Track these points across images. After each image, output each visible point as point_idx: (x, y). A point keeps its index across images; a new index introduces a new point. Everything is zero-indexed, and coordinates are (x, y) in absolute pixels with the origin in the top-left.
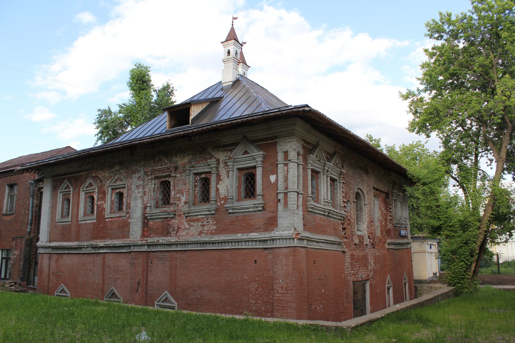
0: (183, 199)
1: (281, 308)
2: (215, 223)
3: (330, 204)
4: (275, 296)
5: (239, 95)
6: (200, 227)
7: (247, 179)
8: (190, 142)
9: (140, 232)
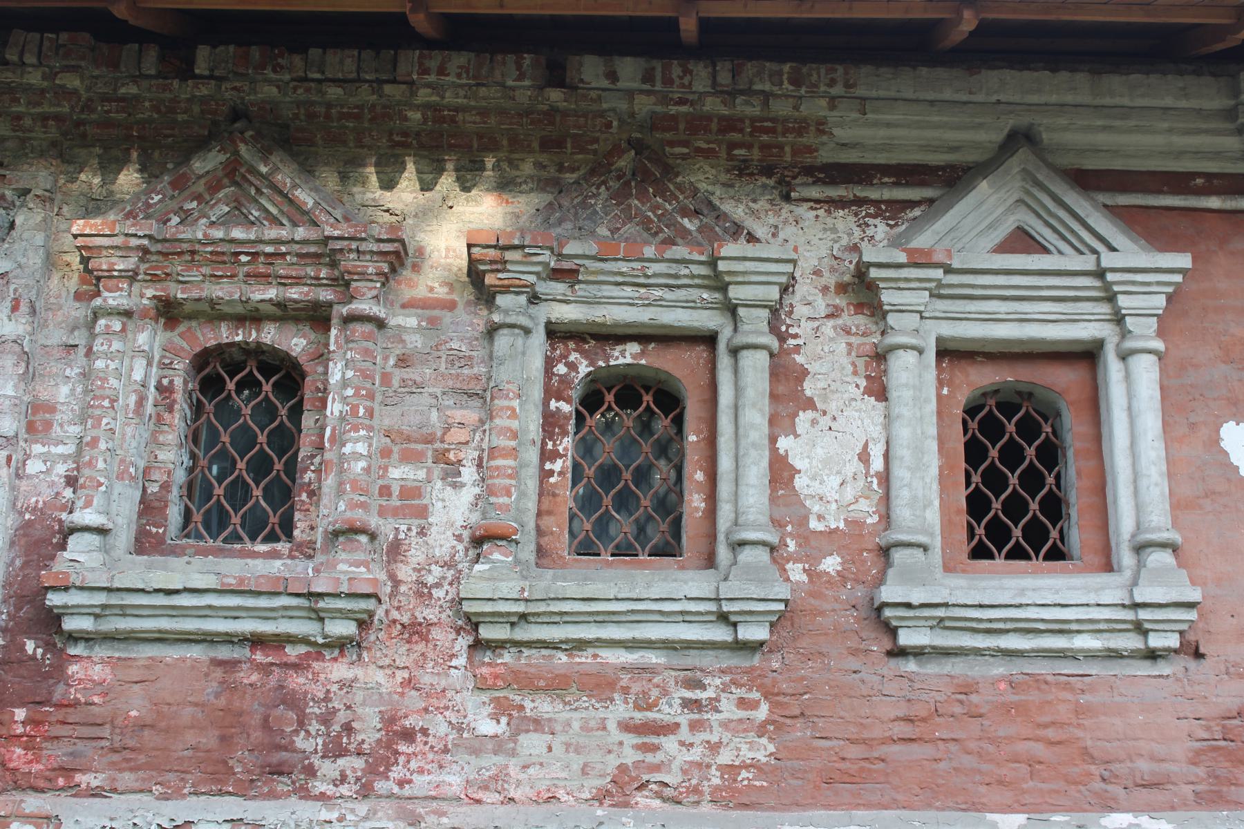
0: (454, 508)
2: (763, 712)
6: (615, 735)
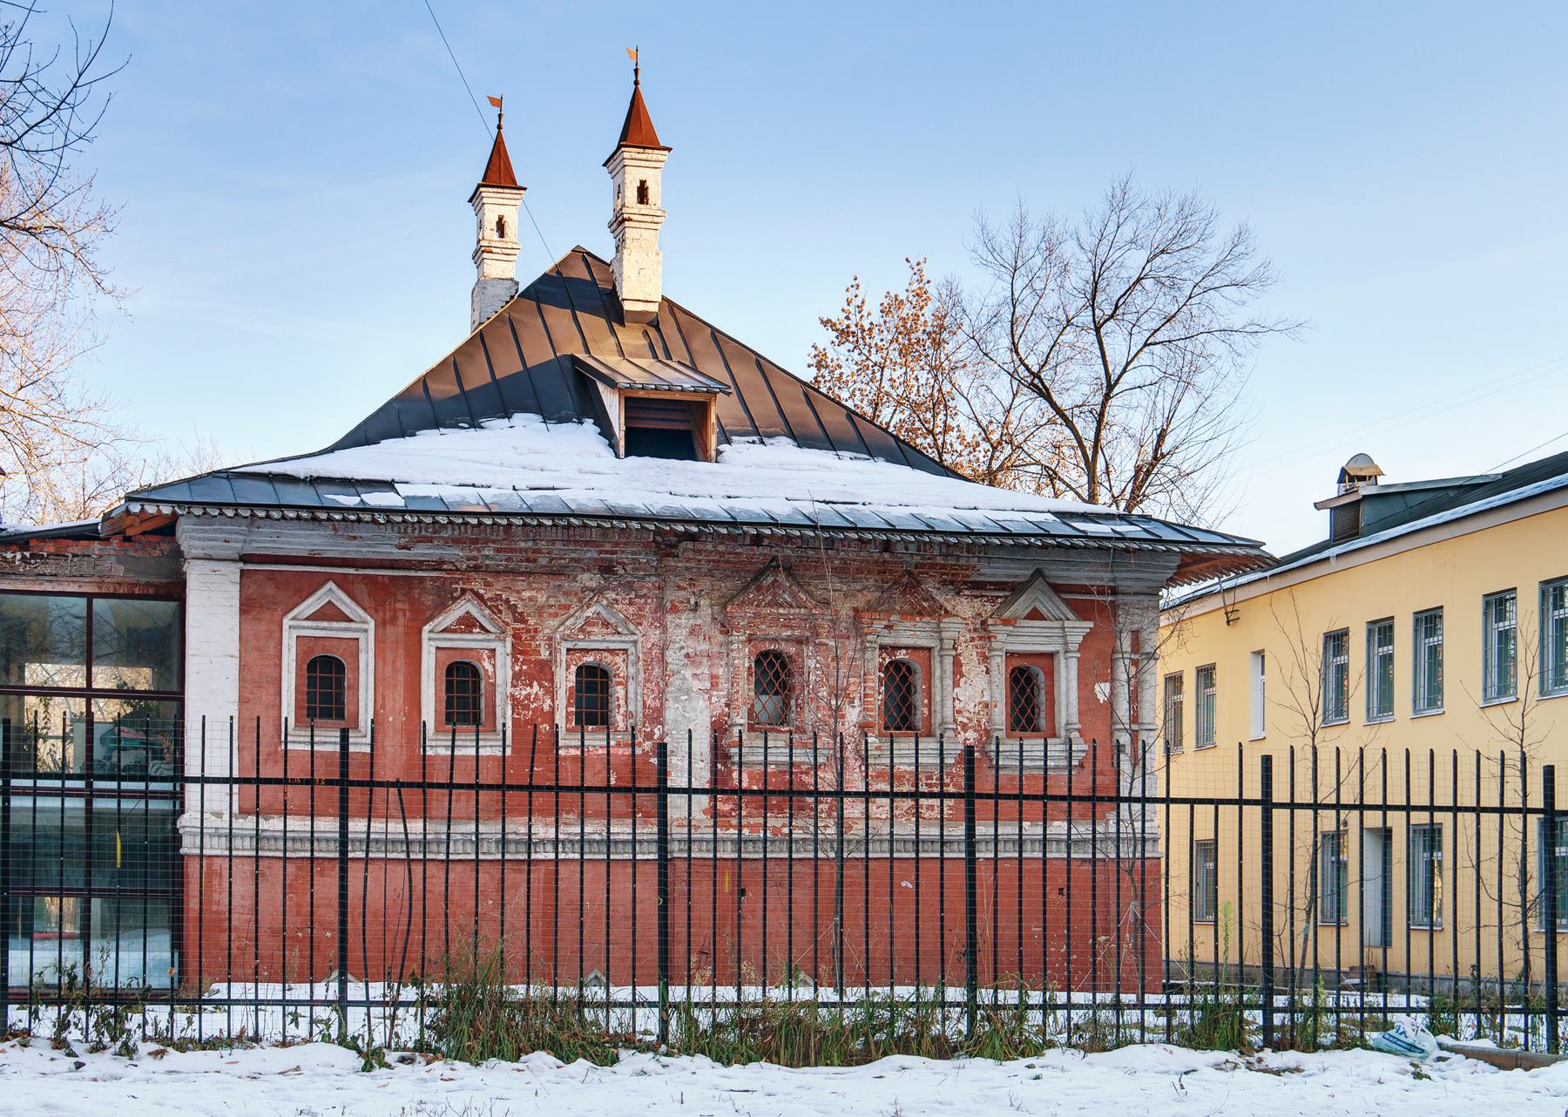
5: (621, 932)
7: (758, 662)
8: (886, 555)
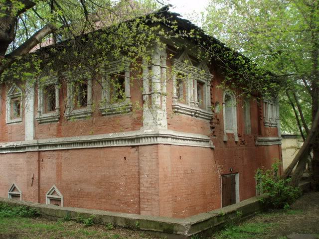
1: (146, 200)
3: (197, 105)
4: (142, 190)
9: (32, 134)
